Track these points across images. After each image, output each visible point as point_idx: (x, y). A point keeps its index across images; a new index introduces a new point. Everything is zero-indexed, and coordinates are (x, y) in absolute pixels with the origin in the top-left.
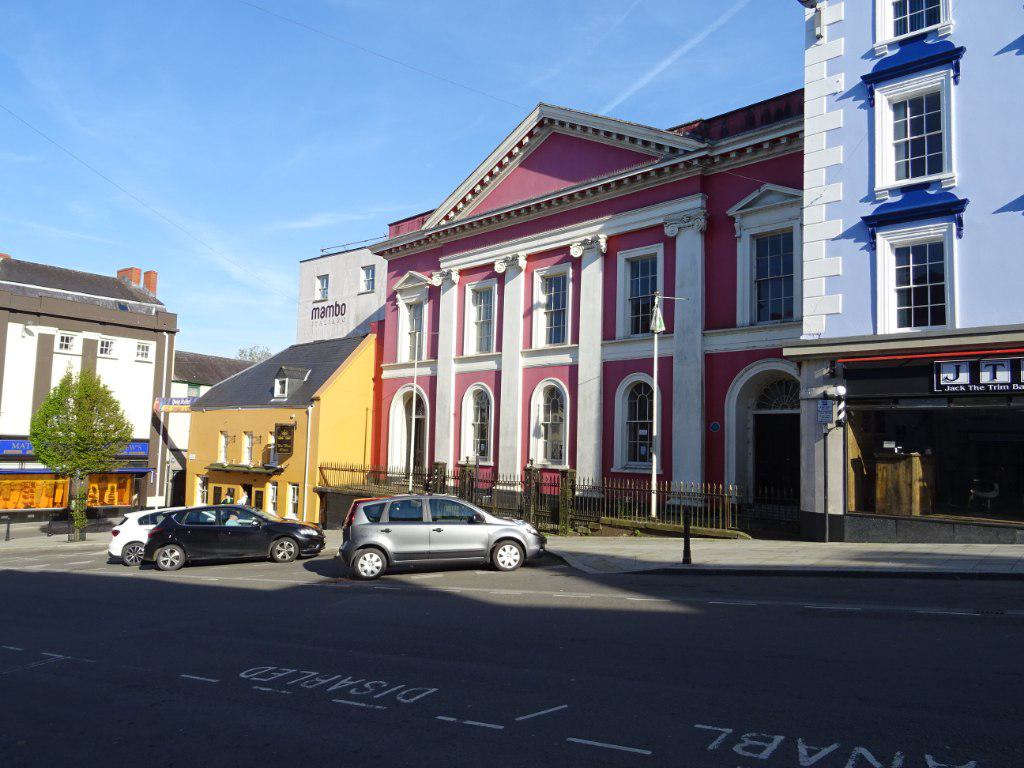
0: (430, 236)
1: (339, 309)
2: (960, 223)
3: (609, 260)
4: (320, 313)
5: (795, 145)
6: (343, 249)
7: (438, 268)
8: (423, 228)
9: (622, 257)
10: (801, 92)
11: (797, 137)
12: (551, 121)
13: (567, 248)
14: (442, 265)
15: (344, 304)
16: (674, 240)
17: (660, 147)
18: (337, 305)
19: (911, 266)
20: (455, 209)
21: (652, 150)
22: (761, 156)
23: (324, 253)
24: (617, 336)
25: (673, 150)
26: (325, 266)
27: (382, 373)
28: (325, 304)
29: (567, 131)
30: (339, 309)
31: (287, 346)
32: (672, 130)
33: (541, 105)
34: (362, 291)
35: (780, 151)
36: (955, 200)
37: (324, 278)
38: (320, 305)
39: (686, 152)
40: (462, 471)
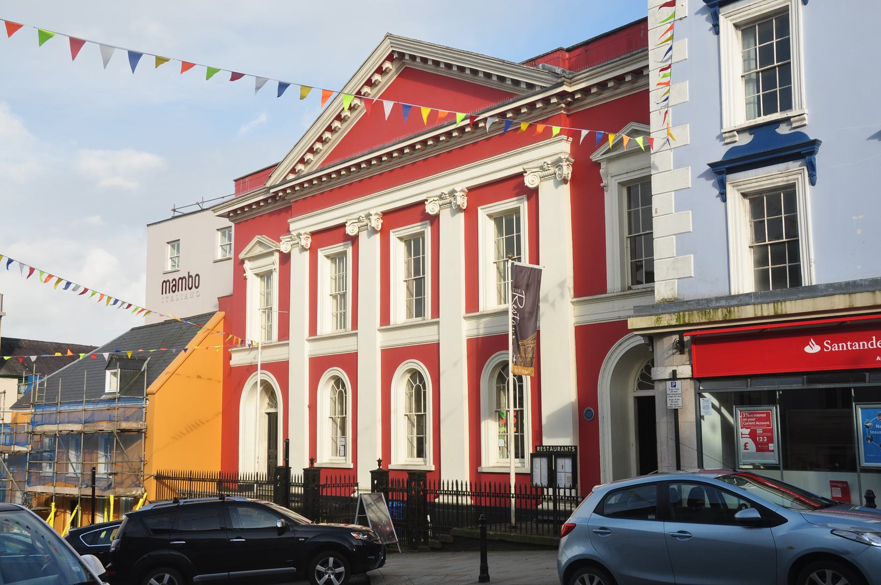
0: (277, 193)
1: (191, 282)
2: (812, 168)
3: (384, 234)
4: (171, 286)
5: (641, 82)
6: (198, 208)
7: (288, 232)
8: (268, 184)
9: (482, 213)
10: (647, 17)
11: (641, 74)
12: (402, 55)
13: (343, 226)
14: (292, 227)
15: (197, 275)
16: (535, 191)
17: (516, 83)
18: (190, 276)
19: (783, 216)
20: (302, 161)
21: (508, 86)
22: (607, 97)
23: (177, 214)
24: (609, 286)
25: (530, 86)
26: (174, 230)
27: (230, 358)
28: (177, 276)
29: (418, 65)
30: (191, 282)
31: (127, 329)
32: (532, 62)
33: (389, 36)
34: (220, 257)
35: (624, 91)
36: (808, 140)
37: (175, 244)
38: (170, 277)
39: (545, 90)
40: (312, 474)
